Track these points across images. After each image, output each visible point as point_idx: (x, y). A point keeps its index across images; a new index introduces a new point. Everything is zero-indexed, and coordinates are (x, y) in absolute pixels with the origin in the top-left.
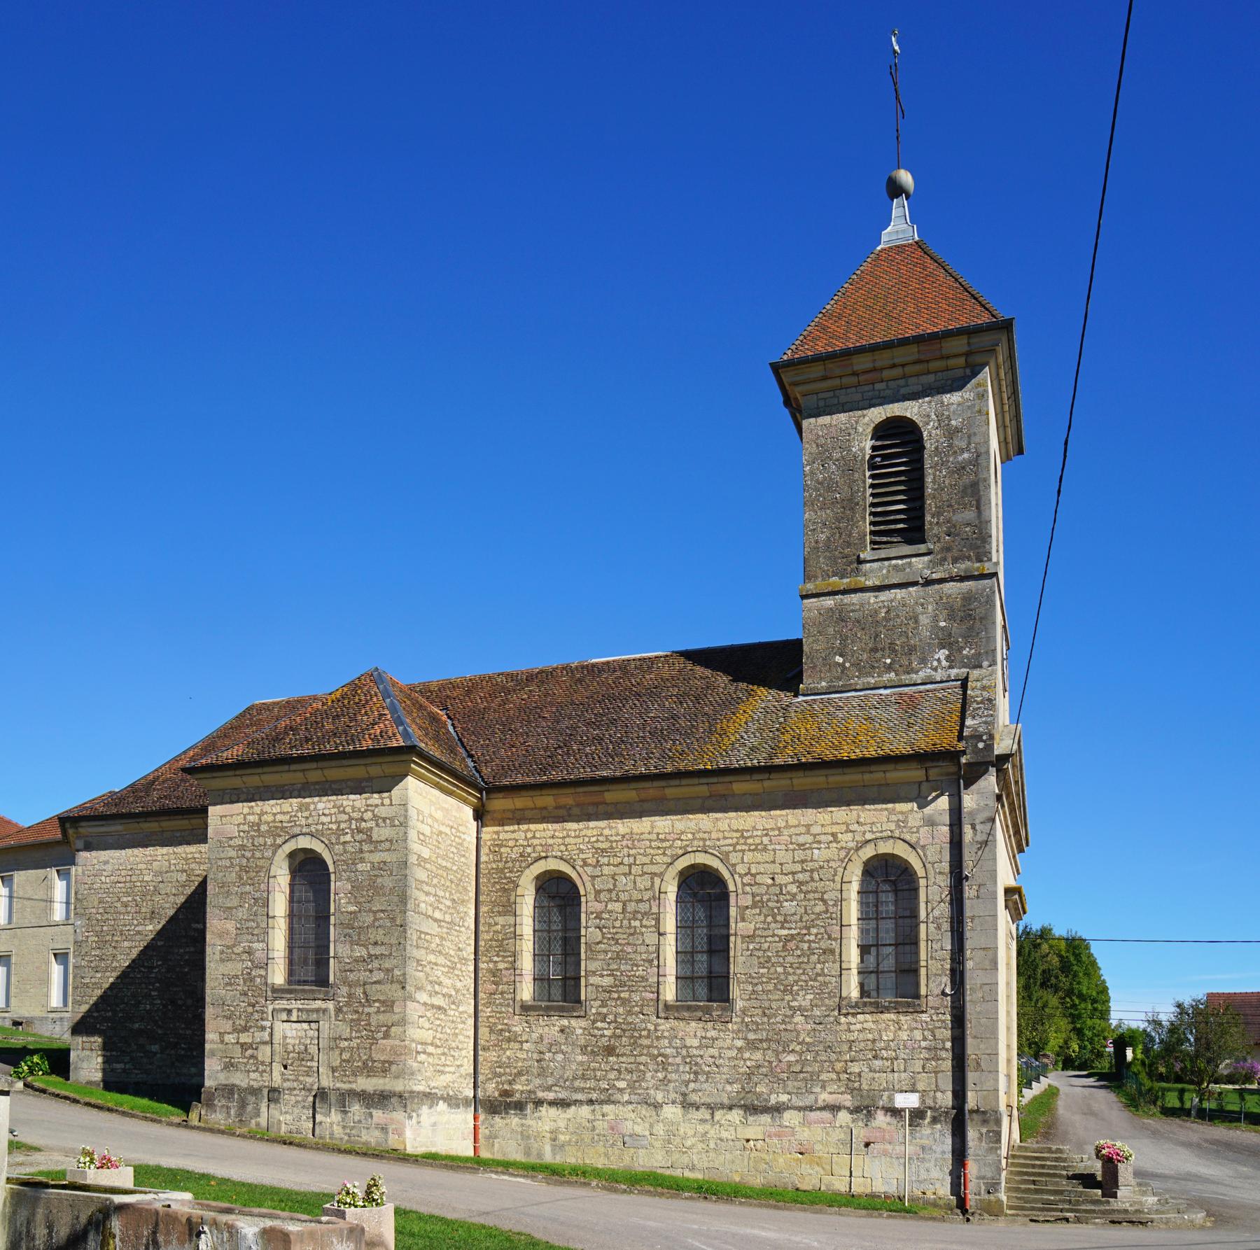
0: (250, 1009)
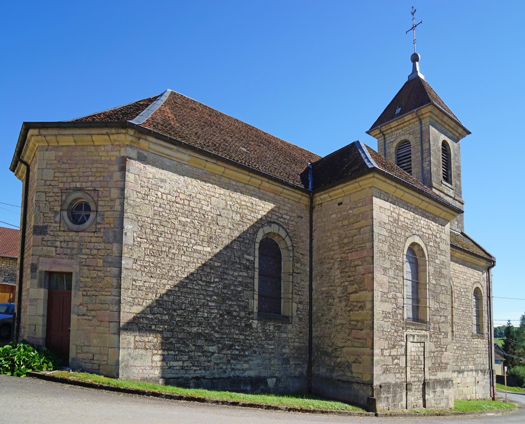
0: (396, 334)
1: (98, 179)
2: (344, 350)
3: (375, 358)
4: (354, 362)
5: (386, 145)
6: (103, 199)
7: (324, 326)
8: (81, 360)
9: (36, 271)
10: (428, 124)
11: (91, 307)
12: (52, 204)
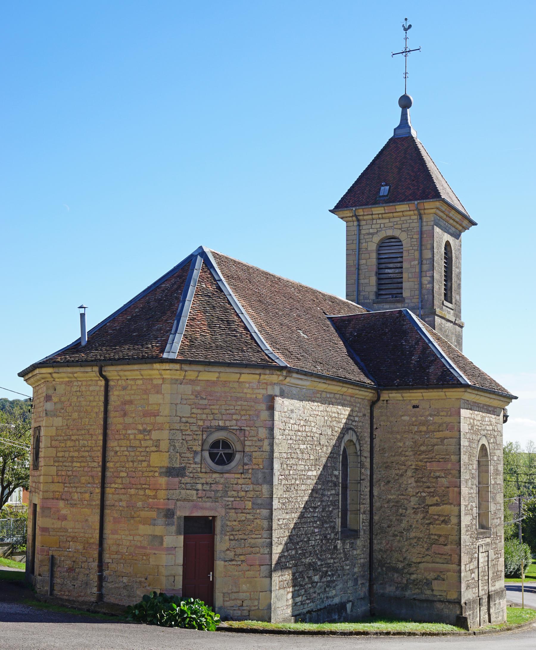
1: (243, 418)
2: (421, 565)
3: (462, 575)
4: (436, 579)
5: (362, 237)
6: (250, 439)
7: (392, 538)
8: (228, 608)
9: (173, 517)
10: (432, 223)
11: (239, 551)
12: (190, 443)
